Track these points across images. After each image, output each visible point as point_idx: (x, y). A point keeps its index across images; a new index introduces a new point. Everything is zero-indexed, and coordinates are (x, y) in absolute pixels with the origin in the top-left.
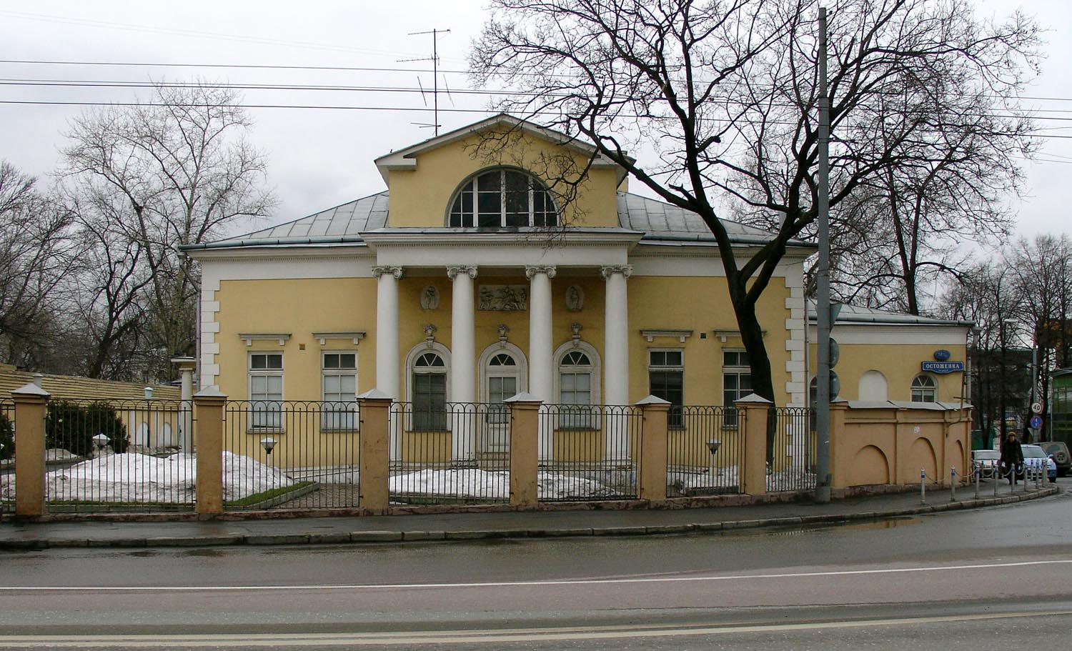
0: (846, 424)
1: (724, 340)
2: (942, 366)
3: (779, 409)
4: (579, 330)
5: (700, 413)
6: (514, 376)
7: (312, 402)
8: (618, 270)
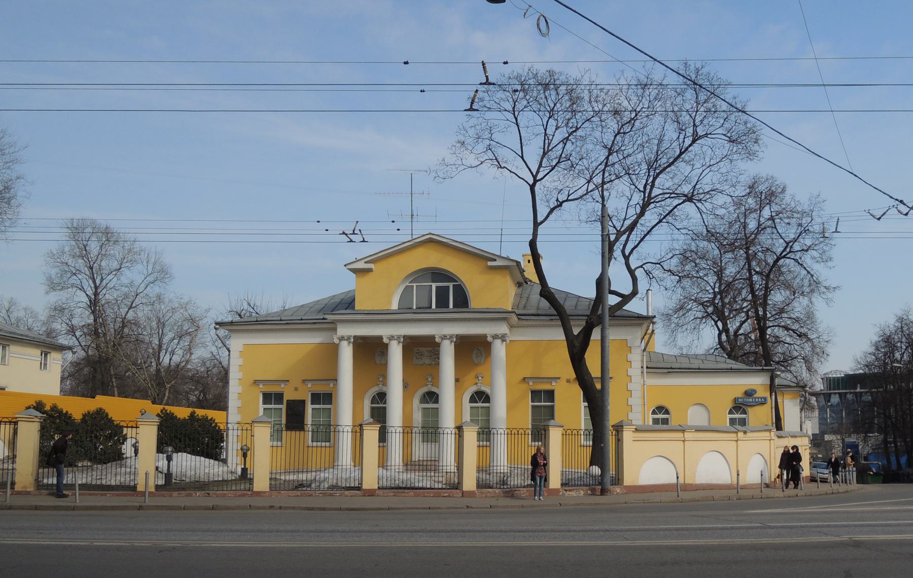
0: (633, 441)
1: (531, 384)
2: (751, 400)
4: (432, 379)
6: (437, 407)
7: (407, 427)
8: (503, 338)
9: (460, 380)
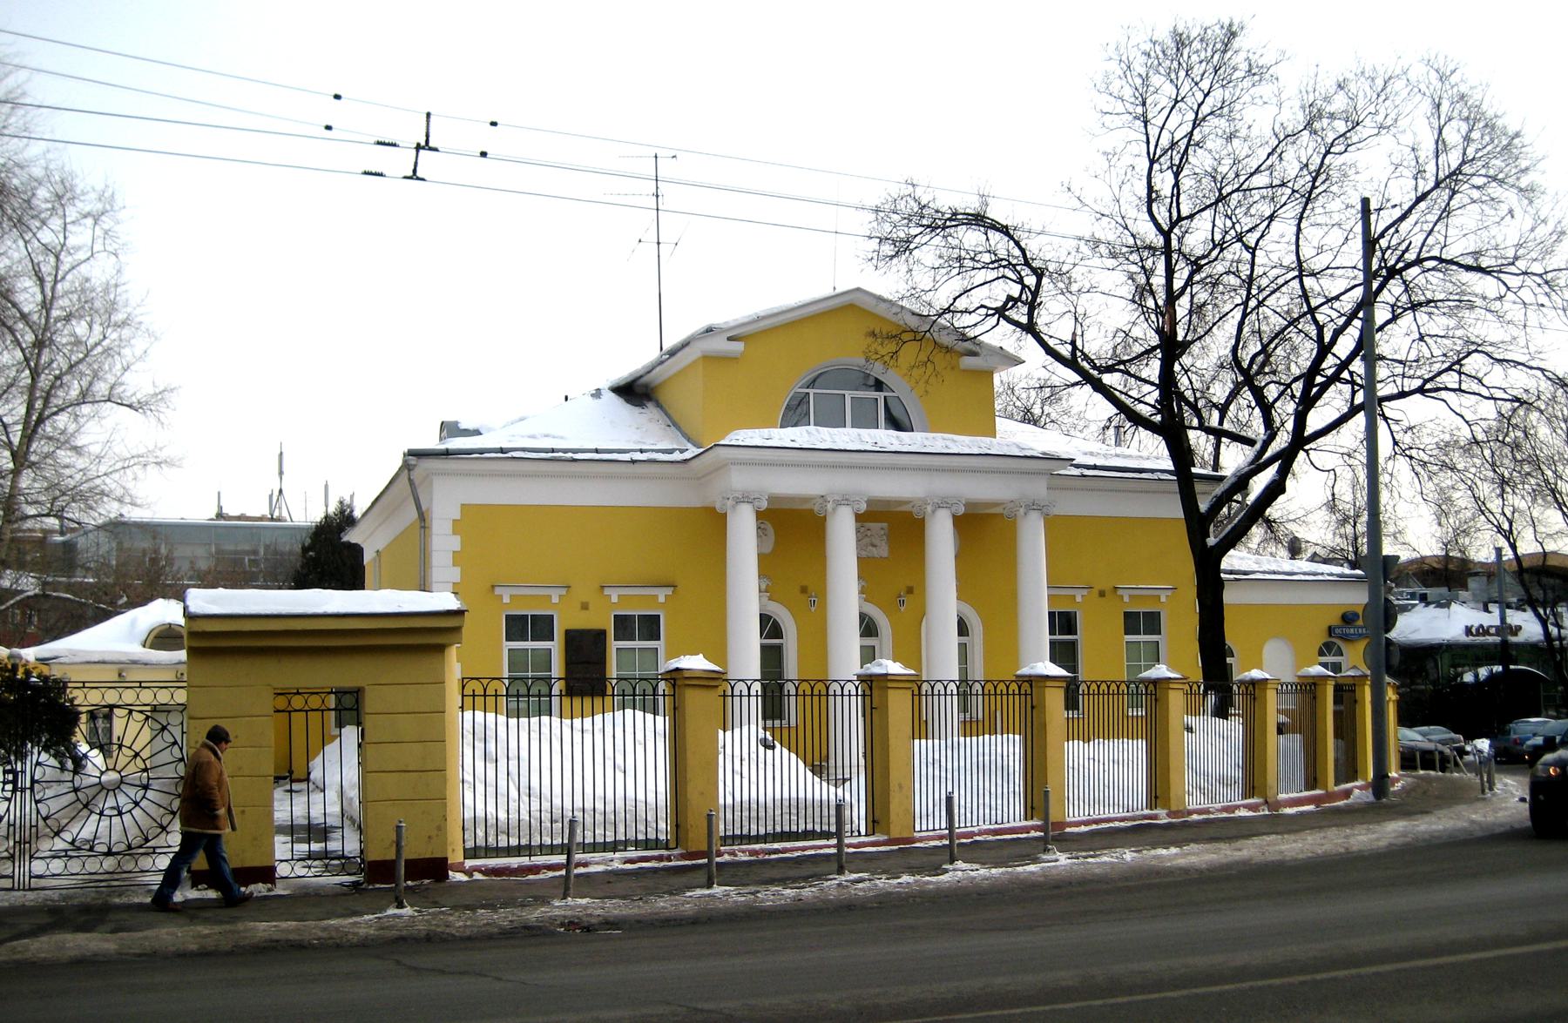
3: (1083, 684)
5: (1011, 692)
7: (472, 679)
8: (1033, 506)
9: (915, 591)
